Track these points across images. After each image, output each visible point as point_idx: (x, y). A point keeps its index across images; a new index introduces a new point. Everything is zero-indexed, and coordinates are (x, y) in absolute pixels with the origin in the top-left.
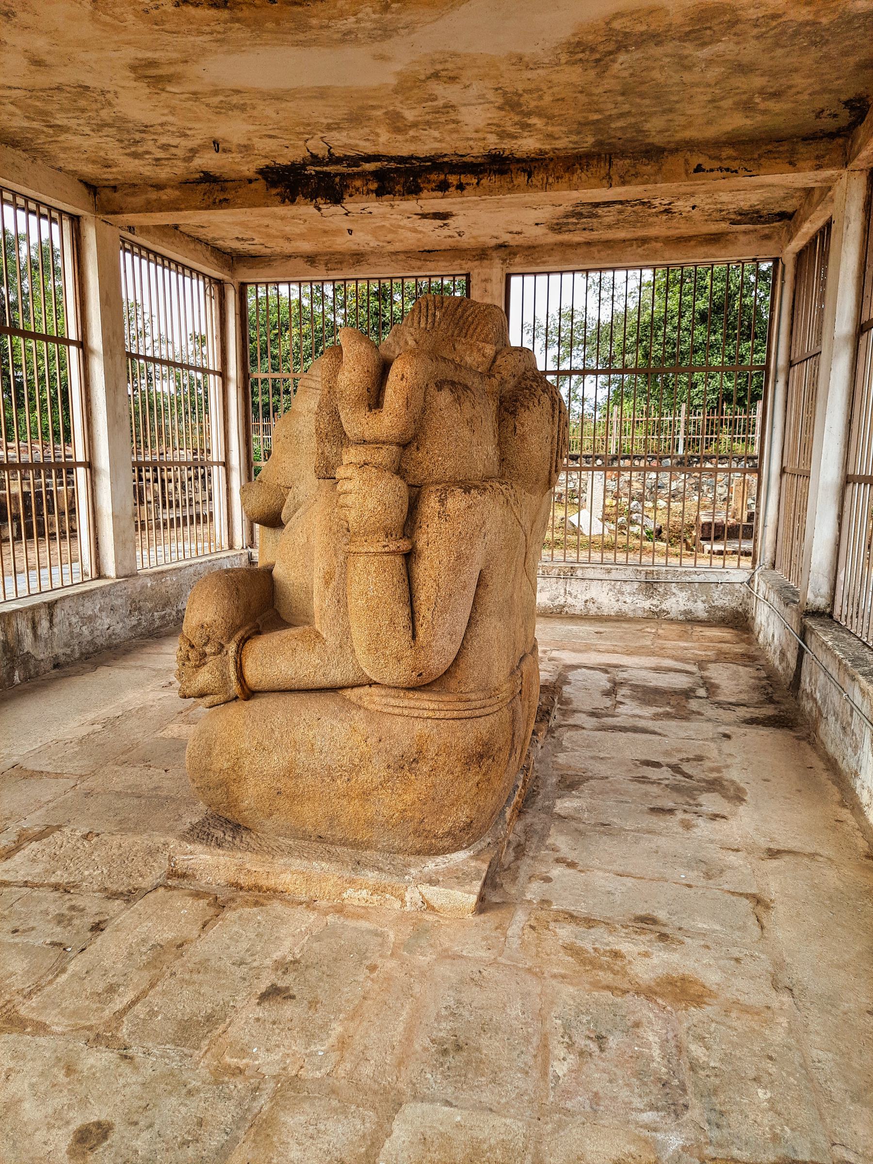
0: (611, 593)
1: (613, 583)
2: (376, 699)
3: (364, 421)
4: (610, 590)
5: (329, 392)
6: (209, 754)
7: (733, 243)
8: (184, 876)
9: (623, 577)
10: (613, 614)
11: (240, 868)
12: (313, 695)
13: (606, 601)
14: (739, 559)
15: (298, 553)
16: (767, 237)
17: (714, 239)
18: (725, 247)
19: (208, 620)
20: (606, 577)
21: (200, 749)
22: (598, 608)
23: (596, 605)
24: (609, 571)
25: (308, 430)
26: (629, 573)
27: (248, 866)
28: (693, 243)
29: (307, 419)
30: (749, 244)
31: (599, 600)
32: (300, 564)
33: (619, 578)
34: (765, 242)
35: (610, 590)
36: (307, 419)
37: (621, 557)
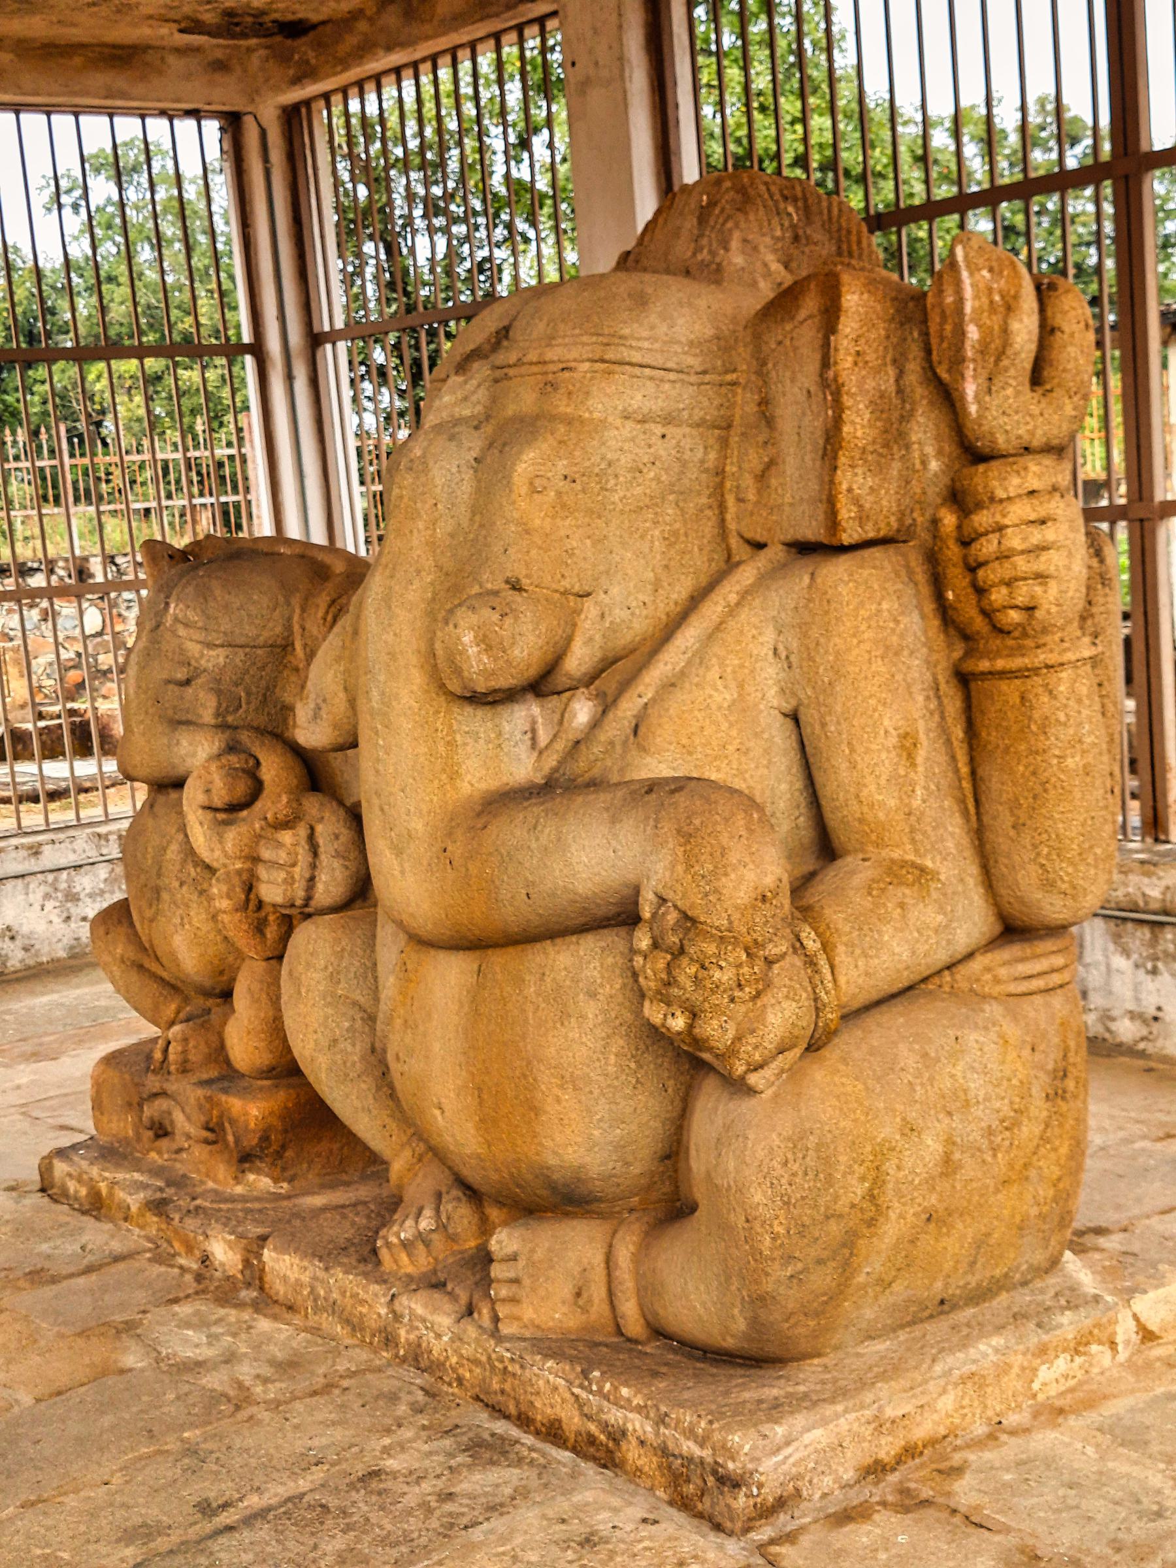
0: (49, 905)
1: (50, 877)
2: (1003, 972)
3: (1035, 410)
4: (47, 896)
5: (856, 364)
6: (830, 1181)
7: (160, 73)
8: (781, 1503)
9: (71, 859)
10: (62, 954)
11: (879, 1425)
12: (884, 1008)
13: (41, 928)
14: (18, 812)
15: (725, 726)
16: (220, 66)
17: (120, 58)
18: (143, 78)
19: (769, 881)
20: (32, 865)
21: (811, 1176)
22: (26, 949)
23: (19, 942)
24: (35, 851)
25: (630, 456)
26: (81, 847)
27: (890, 1412)
28: (78, 60)
29: (626, 432)
30: (188, 77)
31: (25, 929)
32: (731, 748)
33: (63, 862)
34: (217, 77)
35: (47, 896)
36: (626, 432)
37: (61, 814)
